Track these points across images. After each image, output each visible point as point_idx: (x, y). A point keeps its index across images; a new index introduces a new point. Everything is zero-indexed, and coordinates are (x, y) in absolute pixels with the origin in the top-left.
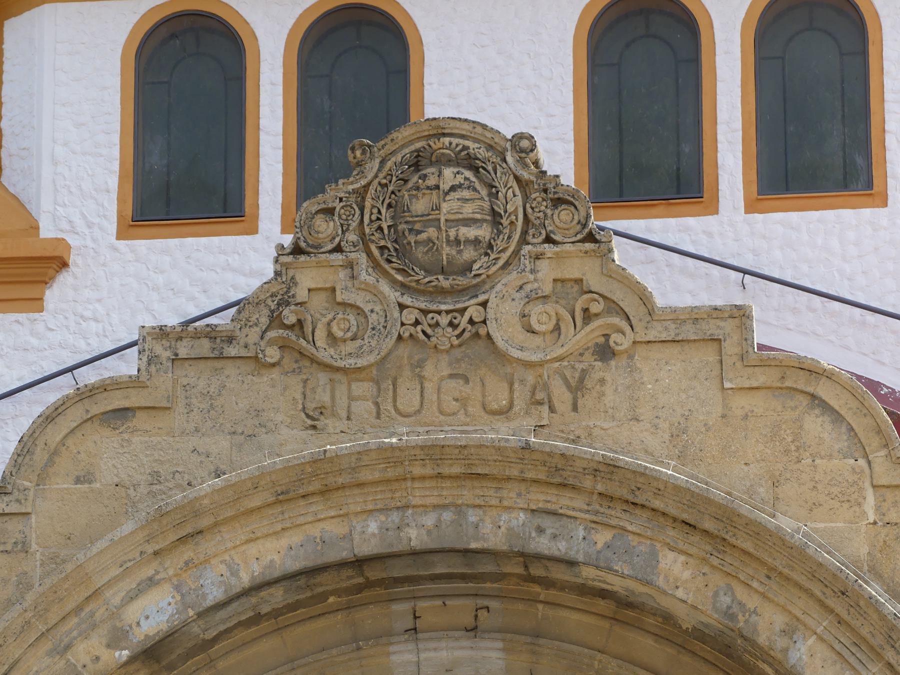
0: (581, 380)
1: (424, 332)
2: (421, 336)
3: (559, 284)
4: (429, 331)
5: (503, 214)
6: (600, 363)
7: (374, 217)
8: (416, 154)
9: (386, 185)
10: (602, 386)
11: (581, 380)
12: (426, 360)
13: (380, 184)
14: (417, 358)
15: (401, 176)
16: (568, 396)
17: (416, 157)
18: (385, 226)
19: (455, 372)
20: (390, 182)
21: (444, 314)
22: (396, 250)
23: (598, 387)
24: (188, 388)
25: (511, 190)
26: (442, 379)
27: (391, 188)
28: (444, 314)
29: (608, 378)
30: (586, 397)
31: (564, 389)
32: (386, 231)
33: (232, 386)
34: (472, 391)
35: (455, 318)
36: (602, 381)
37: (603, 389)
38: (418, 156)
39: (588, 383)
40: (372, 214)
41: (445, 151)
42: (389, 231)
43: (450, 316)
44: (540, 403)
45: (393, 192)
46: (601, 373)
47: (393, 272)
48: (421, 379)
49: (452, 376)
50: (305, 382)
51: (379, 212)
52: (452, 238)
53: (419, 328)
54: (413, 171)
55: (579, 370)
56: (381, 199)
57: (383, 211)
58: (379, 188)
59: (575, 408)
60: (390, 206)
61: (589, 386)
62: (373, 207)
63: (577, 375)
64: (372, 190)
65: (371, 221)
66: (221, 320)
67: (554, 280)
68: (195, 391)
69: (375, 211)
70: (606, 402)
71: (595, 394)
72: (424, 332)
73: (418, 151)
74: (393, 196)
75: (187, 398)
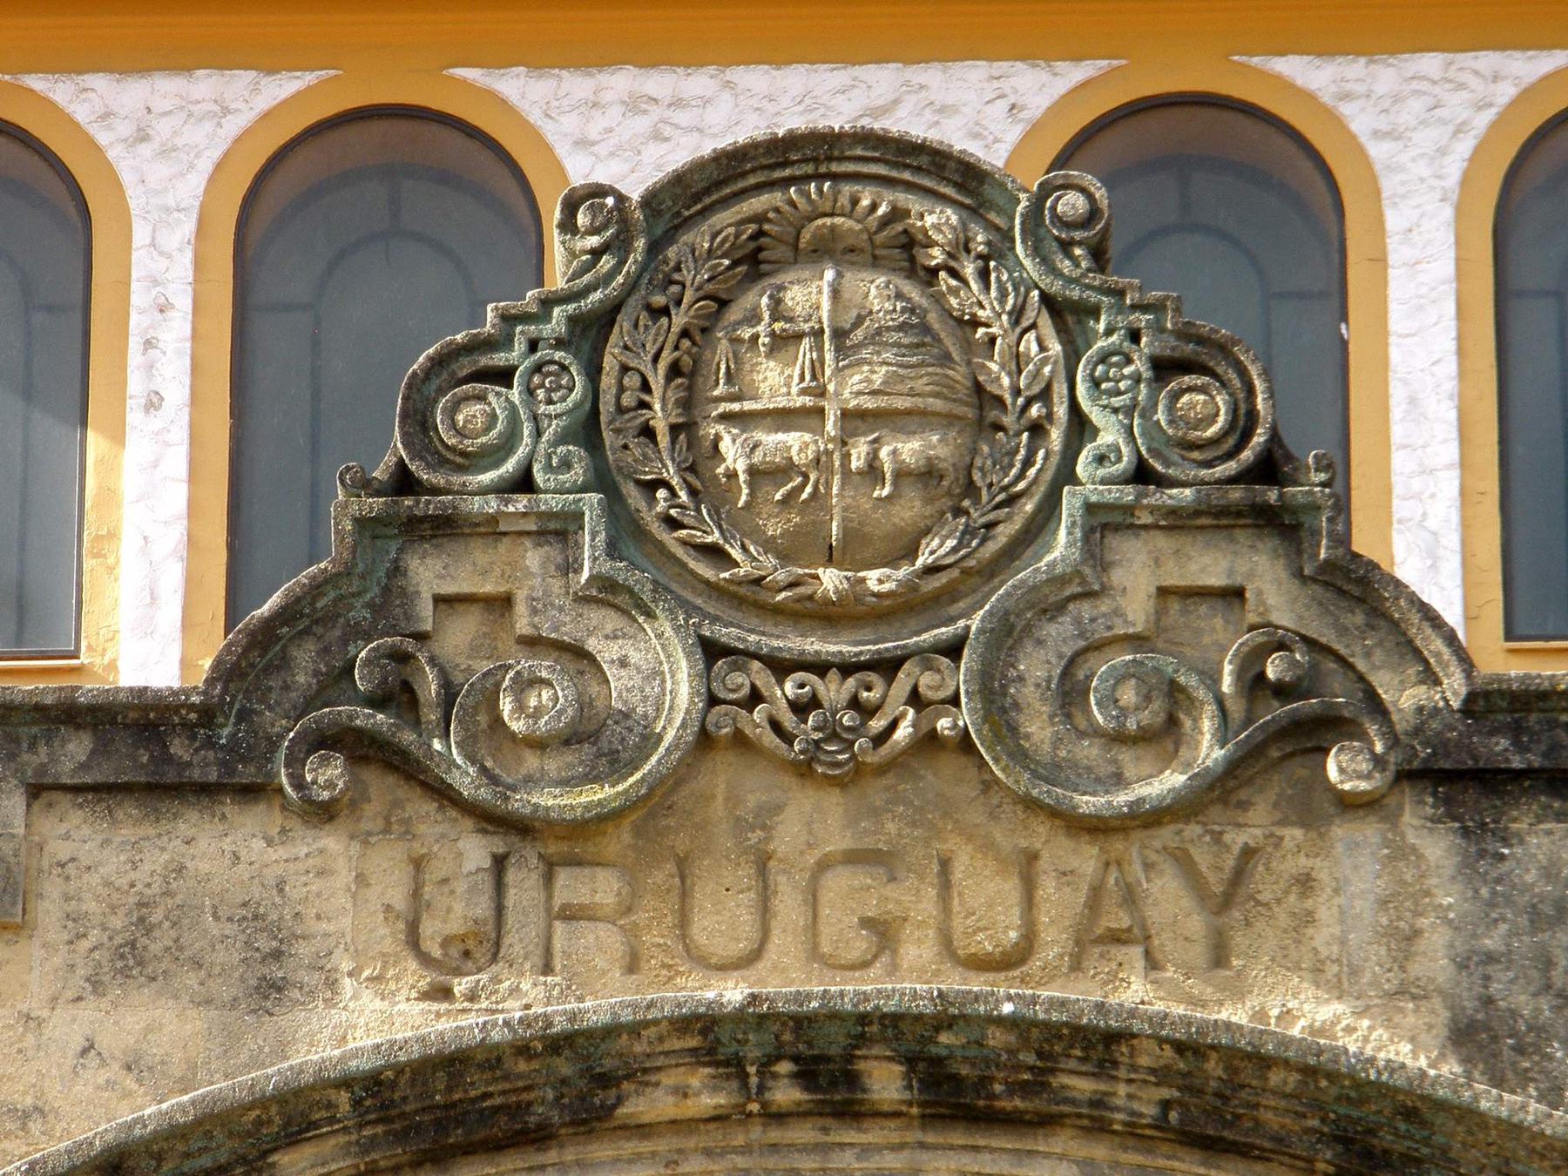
0: (1239, 876)
1: (776, 726)
2: (770, 739)
3: (1175, 606)
4: (788, 720)
5: (1008, 398)
6: (1298, 833)
7: (628, 400)
8: (751, 228)
9: (665, 311)
10: (1303, 895)
11: (1239, 876)
12: (778, 808)
13: (649, 308)
14: (752, 801)
15: (710, 287)
16: (1196, 924)
17: (753, 237)
18: (661, 426)
19: (869, 843)
20: (679, 303)
21: (833, 675)
22: (693, 492)
23: (1292, 898)
24: (71, 869)
25: (1031, 336)
26: (824, 865)
27: (679, 320)
28: (833, 675)
29: (1322, 870)
30: (1259, 925)
31: (1187, 902)
32: (663, 440)
33: (204, 867)
34: (915, 900)
35: (869, 689)
36: (1305, 883)
37: (1309, 904)
38: (760, 233)
39: (1264, 884)
40: (621, 389)
41: (839, 220)
42: (673, 441)
43: (851, 682)
44: (1117, 938)
45: (685, 333)
46: (1302, 860)
47: (680, 552)
48: (762, 863)
49: (853, 858)
50: (418, 864)
51: (646, 387)
52: (856, 463)
53: (759, 714)
54: (746, 275)
55: (1236, 850)
56: (651, 349)
57: (657, 381)
58: (644, 318)
59: (1219, 956)
60: (675, 370)
61: (1265, 896)
62: (625, 369)
63: (1230, 862)
64: (623, 323)
65: (620, 410)
66: (328, 774)
67: (1163, 592)
68: (94, 879)
69: (632, 381)
70: (1317, 943)
71: (1283, 919)
72: (776, 726)
73: (759, 218)
74: (686, 343)
75: (67, 898)
